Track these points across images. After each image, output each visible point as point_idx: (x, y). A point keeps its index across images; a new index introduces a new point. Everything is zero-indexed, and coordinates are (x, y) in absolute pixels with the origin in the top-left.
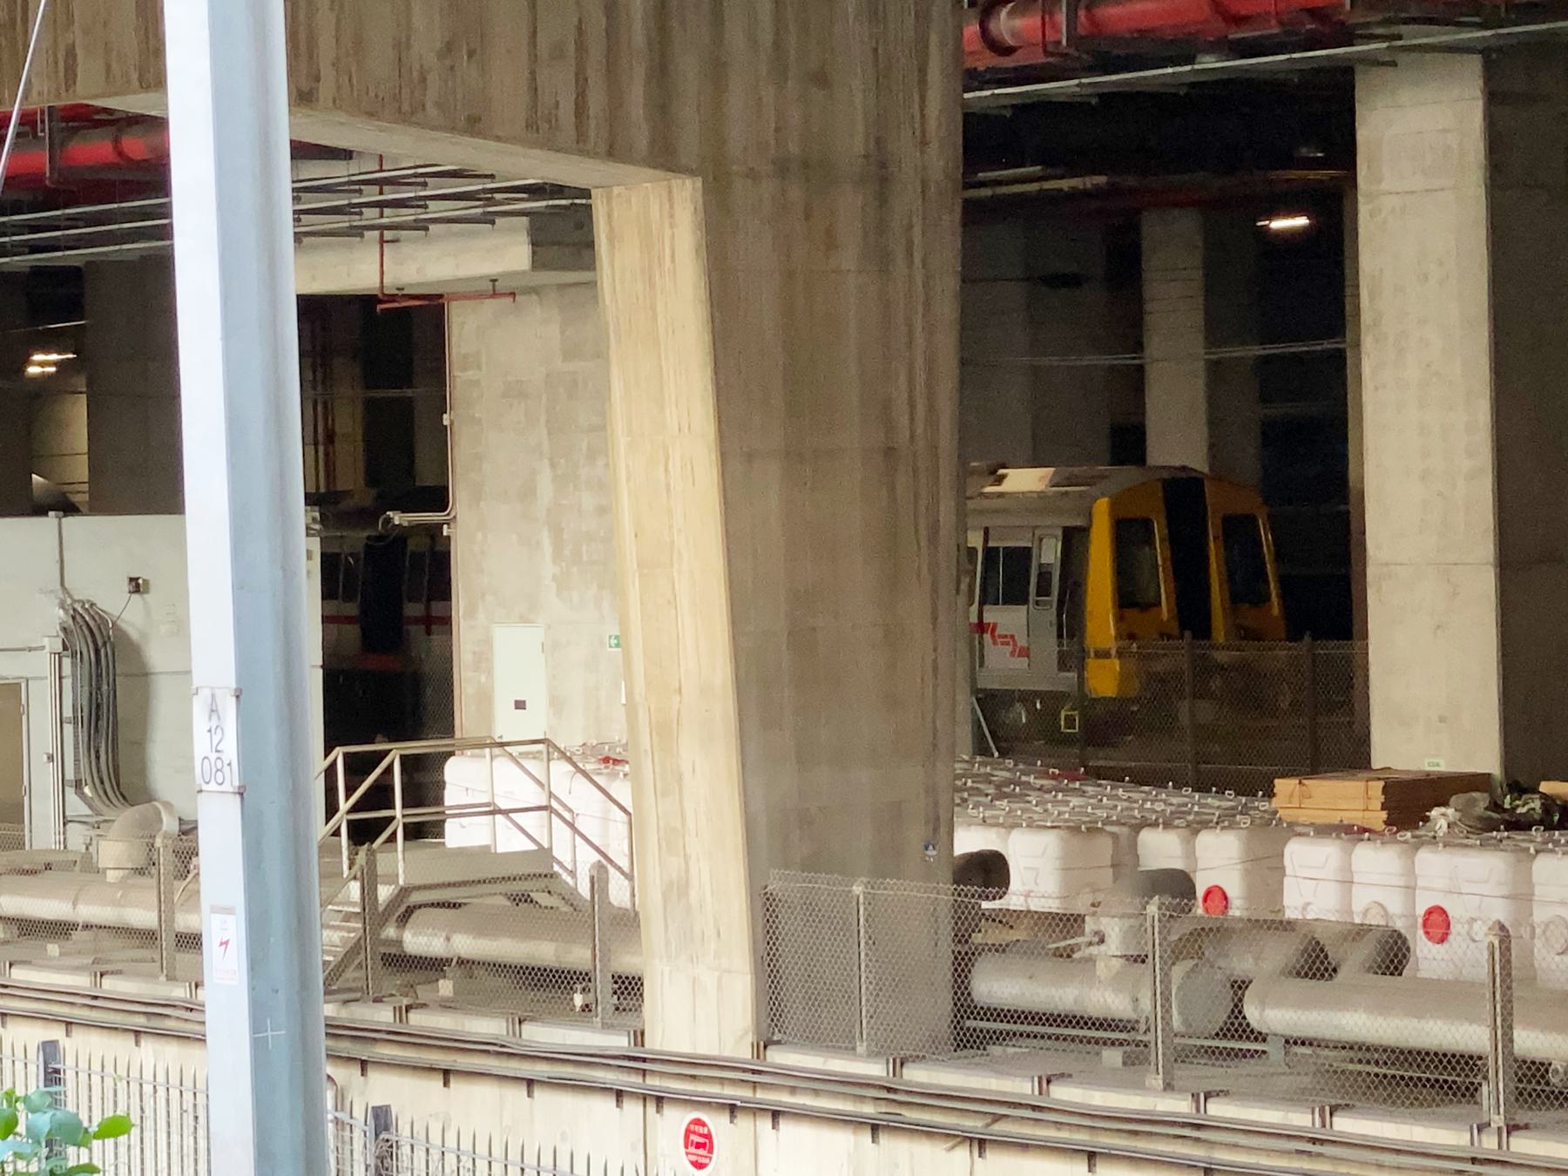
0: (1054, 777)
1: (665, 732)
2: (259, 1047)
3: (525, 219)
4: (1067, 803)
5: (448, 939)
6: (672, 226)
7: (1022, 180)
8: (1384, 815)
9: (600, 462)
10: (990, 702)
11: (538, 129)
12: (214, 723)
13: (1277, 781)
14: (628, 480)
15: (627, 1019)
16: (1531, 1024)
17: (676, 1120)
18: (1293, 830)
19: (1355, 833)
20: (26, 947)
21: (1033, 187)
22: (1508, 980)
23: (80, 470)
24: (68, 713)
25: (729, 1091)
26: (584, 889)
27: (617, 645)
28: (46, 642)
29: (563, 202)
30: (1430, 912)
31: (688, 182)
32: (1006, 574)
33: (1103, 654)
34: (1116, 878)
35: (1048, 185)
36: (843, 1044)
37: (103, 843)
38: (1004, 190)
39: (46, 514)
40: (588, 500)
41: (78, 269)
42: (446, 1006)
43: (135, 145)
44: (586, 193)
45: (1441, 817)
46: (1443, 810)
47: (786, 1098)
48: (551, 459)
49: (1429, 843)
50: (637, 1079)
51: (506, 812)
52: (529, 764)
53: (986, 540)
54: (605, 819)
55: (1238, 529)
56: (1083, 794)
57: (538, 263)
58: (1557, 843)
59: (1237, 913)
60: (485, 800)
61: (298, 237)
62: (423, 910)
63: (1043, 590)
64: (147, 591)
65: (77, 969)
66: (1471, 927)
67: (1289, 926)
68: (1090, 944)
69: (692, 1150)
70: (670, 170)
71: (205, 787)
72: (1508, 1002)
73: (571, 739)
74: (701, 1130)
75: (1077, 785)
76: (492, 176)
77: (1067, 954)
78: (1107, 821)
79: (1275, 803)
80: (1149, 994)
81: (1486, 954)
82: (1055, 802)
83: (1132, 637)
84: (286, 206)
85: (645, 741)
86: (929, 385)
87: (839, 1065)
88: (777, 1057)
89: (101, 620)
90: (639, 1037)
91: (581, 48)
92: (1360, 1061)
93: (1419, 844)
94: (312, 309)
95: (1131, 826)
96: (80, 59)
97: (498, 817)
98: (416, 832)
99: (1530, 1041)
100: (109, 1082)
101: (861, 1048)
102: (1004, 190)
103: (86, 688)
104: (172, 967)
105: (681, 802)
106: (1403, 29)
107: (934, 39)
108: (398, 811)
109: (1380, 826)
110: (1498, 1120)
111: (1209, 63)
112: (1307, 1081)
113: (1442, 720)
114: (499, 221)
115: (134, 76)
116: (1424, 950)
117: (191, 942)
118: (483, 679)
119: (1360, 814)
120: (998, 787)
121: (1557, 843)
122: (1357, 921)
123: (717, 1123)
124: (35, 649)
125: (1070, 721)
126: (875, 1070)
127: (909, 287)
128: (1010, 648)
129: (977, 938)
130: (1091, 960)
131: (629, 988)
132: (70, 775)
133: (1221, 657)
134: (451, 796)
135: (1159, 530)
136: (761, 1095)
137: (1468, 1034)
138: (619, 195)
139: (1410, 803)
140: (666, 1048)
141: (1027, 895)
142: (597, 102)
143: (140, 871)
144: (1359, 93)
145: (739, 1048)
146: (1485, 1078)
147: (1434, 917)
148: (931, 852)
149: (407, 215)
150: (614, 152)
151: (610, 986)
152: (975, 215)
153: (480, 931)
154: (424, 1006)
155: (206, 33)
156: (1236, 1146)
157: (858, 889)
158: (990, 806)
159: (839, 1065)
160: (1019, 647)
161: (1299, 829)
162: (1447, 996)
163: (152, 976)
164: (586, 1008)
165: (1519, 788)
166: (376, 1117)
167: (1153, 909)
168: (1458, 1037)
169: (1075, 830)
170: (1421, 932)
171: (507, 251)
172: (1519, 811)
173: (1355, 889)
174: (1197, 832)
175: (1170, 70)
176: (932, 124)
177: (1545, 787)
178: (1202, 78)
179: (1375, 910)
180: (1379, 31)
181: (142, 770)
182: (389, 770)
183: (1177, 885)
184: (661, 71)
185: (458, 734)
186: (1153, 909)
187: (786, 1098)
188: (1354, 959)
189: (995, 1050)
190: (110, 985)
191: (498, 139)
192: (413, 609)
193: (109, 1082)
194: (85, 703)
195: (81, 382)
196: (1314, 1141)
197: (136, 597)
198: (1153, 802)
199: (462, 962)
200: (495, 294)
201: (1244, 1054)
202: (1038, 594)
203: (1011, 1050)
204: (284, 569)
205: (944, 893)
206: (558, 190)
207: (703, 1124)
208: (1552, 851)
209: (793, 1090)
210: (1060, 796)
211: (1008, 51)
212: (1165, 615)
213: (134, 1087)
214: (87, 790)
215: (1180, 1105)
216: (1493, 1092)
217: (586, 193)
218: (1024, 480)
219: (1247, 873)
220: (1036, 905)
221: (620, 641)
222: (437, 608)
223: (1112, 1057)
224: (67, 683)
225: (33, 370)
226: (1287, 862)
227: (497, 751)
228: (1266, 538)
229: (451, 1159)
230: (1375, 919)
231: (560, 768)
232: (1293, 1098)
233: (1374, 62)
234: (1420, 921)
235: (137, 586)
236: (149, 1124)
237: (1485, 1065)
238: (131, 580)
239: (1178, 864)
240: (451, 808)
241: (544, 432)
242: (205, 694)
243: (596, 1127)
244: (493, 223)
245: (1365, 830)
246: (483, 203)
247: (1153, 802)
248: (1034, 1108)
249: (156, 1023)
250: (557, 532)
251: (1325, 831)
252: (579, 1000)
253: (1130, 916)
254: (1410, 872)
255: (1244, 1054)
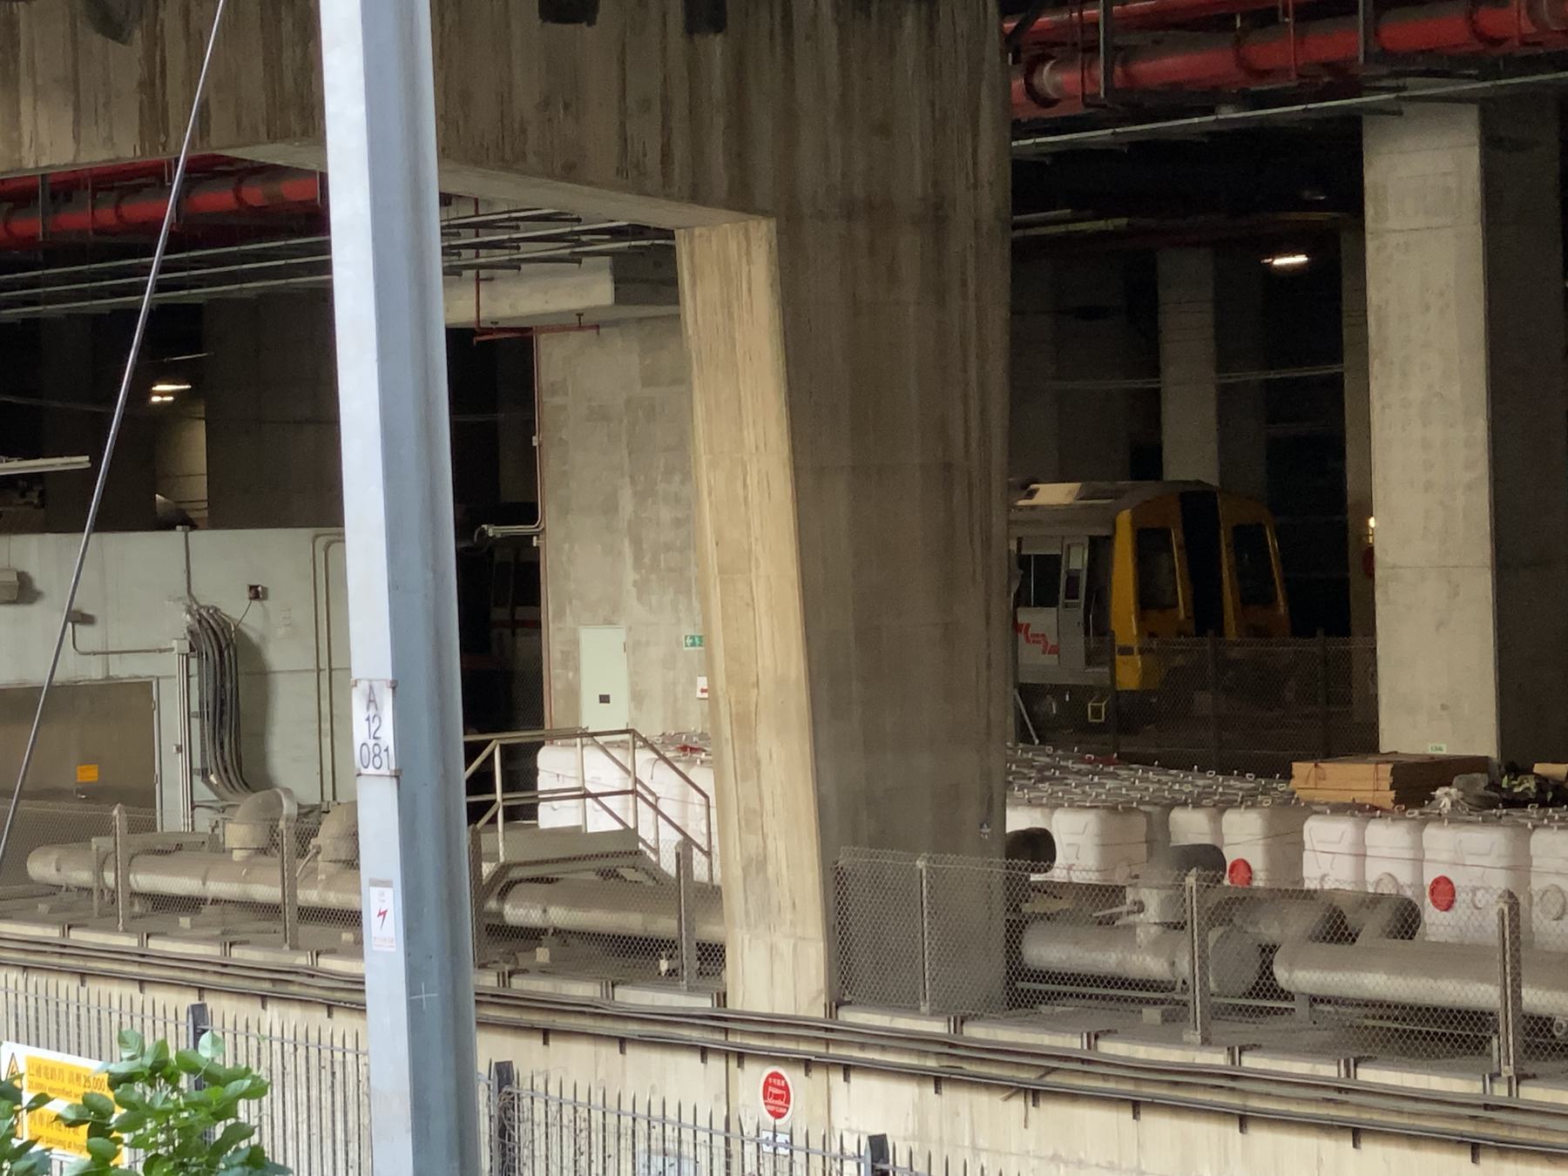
0: (1090, 762)
1: (745, 723)
2: (414, 1008)
3: (608, 258)
4: (1103, 785)
5: (545, 911)
6: (749, 263)
7: (1056, 222)
8: (1392, 794)
9: (677, 478)
10: (1029, 693)
11: (629, 175)
12: (372, 712)
13: (1295, 765)
14: (710, 494)
15: (703, 983)
16: (1533, 985)
17: (753, 1076)
18: (1310, 809)
19: (1366, 811)
20: (159, 921)
21: (1062, 228)
22: (1515, 945)
23: (198, 488)
24: (195, 708)
25: (804, 1047)
26: (668, 864)
27: (693, 645)
28: (175, 644)
29: (644, 243)
30: (1437, 881)
31: (764, 223)
32: (1038, 580)
33: (1127, 651)
34: (1150, 853)
35: (1072, 227)
36: (909, 1006)
37: (229, 826)
38: (1032, 232)
39: (173, 528)
40: (666, 514)
41: (200, 305)
42: (544, 971)
43: (290, 190)
44: (669, 234)
45: (1445, 797)
46: (1447, 789)
47: (856, 1053)
48: (632, 477)
49: (1433, 820)
50: (720, 1037)
51: (595, 796)
52: (616, 753)
53: (1019, 549)
54: (684, 802)
55: (1248, 538)
56: (1115, 776)
57: (620, 298)
58: (1551, 819)
59: (1261, 884)
60: (574, 784)
61: (447, 272)
62: (518, 886)
63: (1072, 593)
64: (265, 598)
65: (208, 940)
66: (1474, 894)
67: (1310, 895)
68: (1128, 913)
69: (770, 1100)
70: (745, 210)
71: (364, 771)
72: (1517, 961)
73: (652, 729)
74: (778, 1082)
75: (1112, 769)
76: (578, 220)
77: (1110, 921)
78: (1141, 801)
79: (1293, 784)
80: (1187, 958)
81: (1496, 919)
82: (1092, 784)
83: (1152, 635)
84: (436, 243)
85: (726, 731)
86: (983, 411)
87: (904, 1023)
88: (850, 1016)
89: (225, 624)
90: (722, 998)
91: (666, 101)
92: (1381, 1018)
93: (1425, 821)
94: (458, 338)
95: (1164, 806)
96: (213, 113)
97: (589, 801)
98: (512, 814)
99: (1535, 998)
100: (253, 1042)
101: (924, 1008)
102: (1032, 232)
103: (211, 685)
104: (295, 937)
105: (759, 786)
106: (1410, 81)
107: (985, 91)
108: (499, 796)
109: (1389, 805)
110: (1508, 1070)
111: (1228, 113)
112: (1326, 1035)
113: (1443, 707)
114: (585, 260)
115: (263, 130)
116: (1433, 917)
117: (352, 918)
118: (571, 675)
119: (1370, 795)
120: (1041, 770)
121: (1551, 819)
122: (1371, 890)
123: (793, 1077)
124: (165, 651)
125: (1097, 713)
126: (938, 1027)
127: (962, 321)
128: (1041, 646)
129: (1026, 908)
130: (1131, 928)
131: (712, 956)
132: (197, 764)
133: (1235, 653)
134: (544, 782)
135: (1176, 538)
136: (832, 1051)
137: (1483, 994)
138: (701, 236)
139: (1416, 785)
140: (747, 1008)
141: (1070, 868)
142: (680, 151)
143: (263, 851)
144: (1367, 141)
145: (816, 1011)
146: (1496, 1032)
147: (1440, 887)
148: (986, 830)
149: (501, 256)
150: (696, 195)
151: (695, 953)
152: (1022, 253)
153: (574, 902)
154: (525, 971)
155: (361, 82)
156: (1268, 1095)
157: (920, 864)
158: (1033, 788)
159: (904, 1023)
160: (1050, 642)
161: (1315, 808)
162: (1459, 957)
163: (276, 946)
164: (672, 973)
165: (1516, 769)
166: (499, 1072)
167: (1191, 880)
168: (1471, 995)
169: (1113, 809)
170: (1428, 900)
171: (593, 289)
172: (1516, 790)
173: (1368, 861)
174: (1223, 811)
175: (1196, 120)
176: (985, 171)
177: (1539, 768)
178: (1225, 128)
179: (1386, 880)
180: (1384, 83)
181: (262, 758)
182: (491, 756)
183: (1209, 858)
184: (739, 127)
185: (547, 726)
186: (1191, 880)
187: (856, 1053)
188: (1371, 927)
189: (1044, 1009)
190: (237, 953)
191: (590, 184)
192: (500, 614)
193: (253, 1042)
194: (211, 698)
195: (201, 409)
196: (1340, 1090)
197: (256, 603)
198: (1181, 784)
199: (557, 932)
200: (580, 327)
201: (1263, 1011)
202: (1067, 597)
203: (1058, 1009)
204: (435, 571)
205: (997, 867)
206: (638, 231)
207: (781, 1078)
208: (1547, 826)
209: (863, 1046)
210: (1096, 779)
211: (1048, 103)
212: (1182, 615)
213: (276, 1046)
214: (212, 778)
215: (1219, 1059)
216: (1504, 1045)
217: (669, 234)
218: (1053, 494)
219: (1269, 851)
220: (1077, 878)
221: (702, 640)
222: (522, 613)
223: (1152, 1015)
224: (194, 681)
225: (156, 399)
226: (1306, 837)
227: (585, 740)
228: (1272, 543)
229: (568, 1111)
230: (1387, 889)
231: (644, 756)
232: (1317, 1052)
233: (1379, 111)
234: (1428, 891)
235: (256, 593)
236: (290, 1080)
237: (1496, 1020)
238: (251, 587)
239: (1207, 840)
240: (543, 792)
241: (625, 452)
242: (363, 685)
243: (684, 1083)
244: (580, 262)
245: (1377, 809)
246: (570, 244)
247: (1181, 784)
248: (1083, 1061)
249: (279, 988)
250: (637, 543)
251: (1339, 809)
252: (664, 965)
253: (1171, 887)
254: (1418, 846)
255: (1263, 1011)
